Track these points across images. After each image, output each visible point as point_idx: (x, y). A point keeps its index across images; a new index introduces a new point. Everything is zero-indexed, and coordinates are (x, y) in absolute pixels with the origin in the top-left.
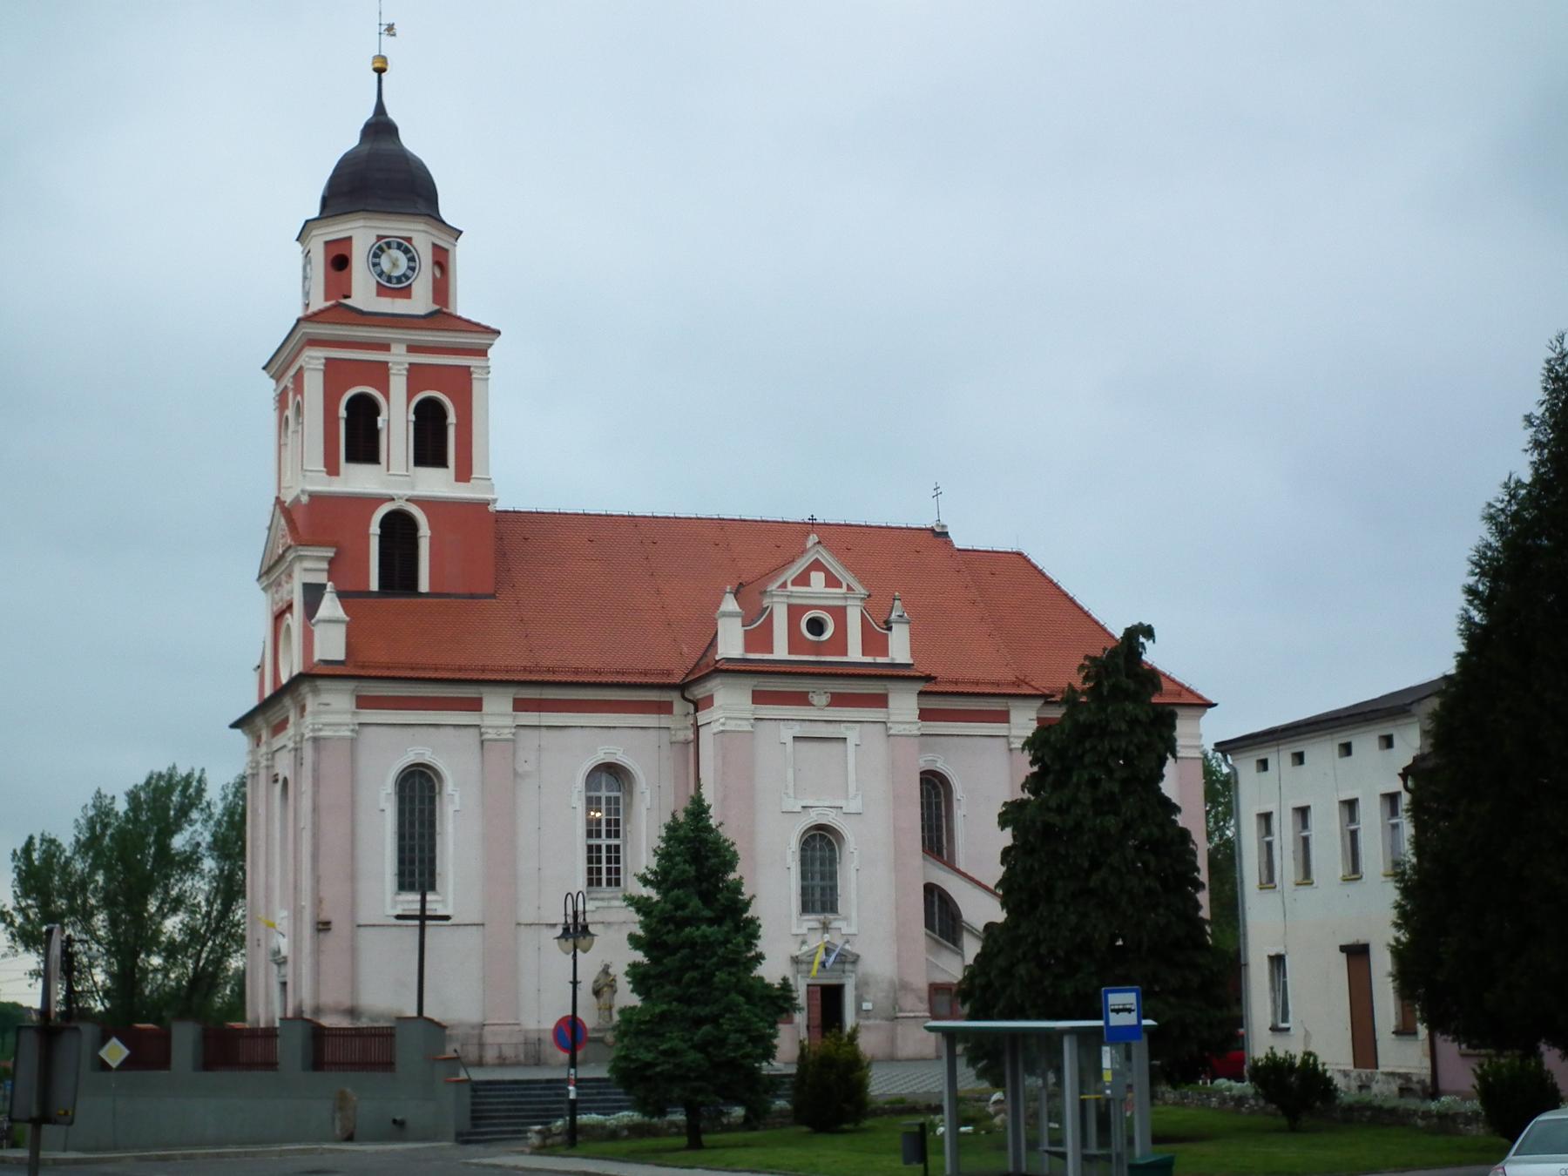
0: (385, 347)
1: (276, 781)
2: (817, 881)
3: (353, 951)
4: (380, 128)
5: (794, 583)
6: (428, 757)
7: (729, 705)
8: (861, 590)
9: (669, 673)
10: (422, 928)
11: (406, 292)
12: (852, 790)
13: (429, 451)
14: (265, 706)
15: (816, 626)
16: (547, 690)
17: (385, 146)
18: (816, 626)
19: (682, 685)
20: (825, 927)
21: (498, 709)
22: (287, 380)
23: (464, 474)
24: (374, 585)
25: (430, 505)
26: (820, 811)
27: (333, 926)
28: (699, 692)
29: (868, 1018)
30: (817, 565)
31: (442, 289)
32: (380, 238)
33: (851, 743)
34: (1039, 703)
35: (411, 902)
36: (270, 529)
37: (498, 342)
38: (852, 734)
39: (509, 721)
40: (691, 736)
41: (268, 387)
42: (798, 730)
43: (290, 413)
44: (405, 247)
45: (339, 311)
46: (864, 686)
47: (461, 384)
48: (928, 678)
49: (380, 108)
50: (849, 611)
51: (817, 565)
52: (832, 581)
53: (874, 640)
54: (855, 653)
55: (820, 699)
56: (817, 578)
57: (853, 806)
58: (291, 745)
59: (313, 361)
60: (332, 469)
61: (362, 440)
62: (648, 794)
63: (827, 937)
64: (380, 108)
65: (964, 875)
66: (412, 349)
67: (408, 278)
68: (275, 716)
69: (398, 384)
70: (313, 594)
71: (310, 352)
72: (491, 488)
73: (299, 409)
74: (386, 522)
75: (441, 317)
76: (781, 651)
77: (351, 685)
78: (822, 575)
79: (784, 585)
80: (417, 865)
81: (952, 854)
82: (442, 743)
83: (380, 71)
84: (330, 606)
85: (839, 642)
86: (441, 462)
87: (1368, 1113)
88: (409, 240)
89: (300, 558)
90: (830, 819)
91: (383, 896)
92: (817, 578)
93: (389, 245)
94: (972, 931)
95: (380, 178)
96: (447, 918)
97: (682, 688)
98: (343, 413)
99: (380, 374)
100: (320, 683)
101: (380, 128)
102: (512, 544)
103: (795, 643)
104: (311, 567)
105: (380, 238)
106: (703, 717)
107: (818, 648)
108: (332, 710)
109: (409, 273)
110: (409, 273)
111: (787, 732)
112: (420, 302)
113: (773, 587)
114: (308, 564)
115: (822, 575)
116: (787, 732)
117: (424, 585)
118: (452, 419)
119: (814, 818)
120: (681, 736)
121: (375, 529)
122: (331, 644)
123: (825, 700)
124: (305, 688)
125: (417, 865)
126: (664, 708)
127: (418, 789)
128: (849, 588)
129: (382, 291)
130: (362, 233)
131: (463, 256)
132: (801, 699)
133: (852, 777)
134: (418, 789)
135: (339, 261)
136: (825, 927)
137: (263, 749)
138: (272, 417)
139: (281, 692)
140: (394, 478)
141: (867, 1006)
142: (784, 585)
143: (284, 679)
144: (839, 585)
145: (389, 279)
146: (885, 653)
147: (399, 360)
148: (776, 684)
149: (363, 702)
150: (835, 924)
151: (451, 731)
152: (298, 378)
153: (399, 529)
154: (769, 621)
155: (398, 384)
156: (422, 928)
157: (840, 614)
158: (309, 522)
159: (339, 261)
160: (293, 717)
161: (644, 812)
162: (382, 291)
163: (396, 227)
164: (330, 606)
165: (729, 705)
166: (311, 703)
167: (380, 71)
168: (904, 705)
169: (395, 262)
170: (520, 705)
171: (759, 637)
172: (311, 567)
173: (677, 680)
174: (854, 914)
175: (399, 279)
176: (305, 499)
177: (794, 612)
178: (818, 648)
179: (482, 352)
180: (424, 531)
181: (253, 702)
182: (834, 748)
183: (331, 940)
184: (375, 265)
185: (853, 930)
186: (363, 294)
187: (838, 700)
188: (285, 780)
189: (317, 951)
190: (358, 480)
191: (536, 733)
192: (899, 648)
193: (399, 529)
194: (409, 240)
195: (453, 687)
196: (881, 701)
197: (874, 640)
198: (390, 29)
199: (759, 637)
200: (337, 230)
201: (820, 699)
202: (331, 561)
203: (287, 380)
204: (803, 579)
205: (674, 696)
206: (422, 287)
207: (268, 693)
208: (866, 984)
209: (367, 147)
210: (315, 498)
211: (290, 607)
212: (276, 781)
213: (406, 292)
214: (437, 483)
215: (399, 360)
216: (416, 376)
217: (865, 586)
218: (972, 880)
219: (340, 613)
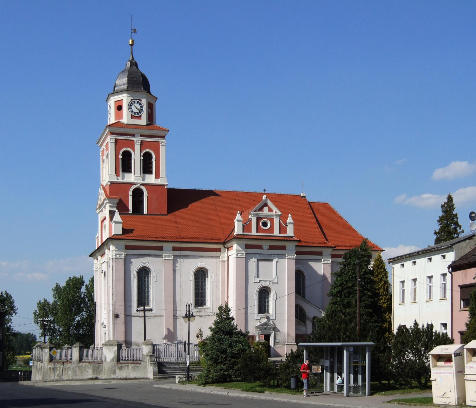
0: (133, 135)
11: (139, 117)
13: (147, 169)
15: (265, 224)
53: (282, 229)
54: (276, 233)
56: (266, 209)
58: (106, 261)
66: (142, 136)
90: (267, 284)
93: (134, 102)
98: (120, 156)
99: (131, 145)
103: (258, 229)
117: (145, 212)
119: (262, 284)
121: (131, 193)
128: (276, 212)
129: (132, 117)
132: (260, 247)
140: (134, 177)
145: (135, 113)
157: (272, 220)
162: (132, 117)
171: (246, 227)
177: (258, 219)
180: (145, 194)
187: (271, 248)
188: (105, 272)
193: (138, 194)
197: (282, 229)
198: (135, 31)
204: (261, 209)
205: (221, 246)
206: (144, 115)
213: (139, 117)
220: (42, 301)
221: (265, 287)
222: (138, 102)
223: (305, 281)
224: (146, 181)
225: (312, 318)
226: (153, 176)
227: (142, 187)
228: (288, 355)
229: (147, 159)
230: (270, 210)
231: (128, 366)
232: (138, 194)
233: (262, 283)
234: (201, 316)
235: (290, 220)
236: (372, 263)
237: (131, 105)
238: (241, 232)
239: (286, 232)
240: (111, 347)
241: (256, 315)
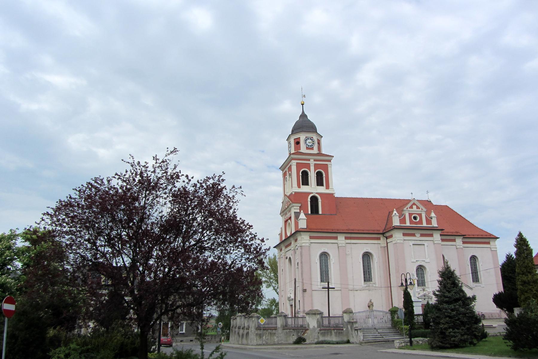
0: (309, 160)
1: (287, 258)
2: (420, 279)
3: (312, 296)
4: (303, 116)
6: (326, 250)
7: (398, 236)
8: (425, 210)
9: (379, 231)
10: (328, 291)
11: (312, 149)
12: (427, 257)
13: (320, 182)
14: (282, 242)
15: (415, 218)
16: (352, 234)
17: (305, 119)
19: (385, 232)
20: (424, 290)
21: (341, 239)
22: (287, 169)
23: (328, 187)
24: (310, 212)
25: (319, 194)
28: (388, 234)
31: (319, 149)
33: (426, 245)
34: (462, 237)
35: (326, 285)
36: (283, 203)
37: (333, 158)
38: (426, 243)
39: (344, 242)
40: (386, 245)
41: (281, 173)
43: (288, 176)
44: (311, 139)
45: (298, 153)
46: (428, 232)
47: (326, 168)
48: (442, 230)
49: (303, 112)
52: (418, 208)
53: (429, 221)
54: (425, 224)
55: (418, 235)
56: (414, 207)
57: (427, 260)
58: (292, 249)
59: (294, 163)
60: (299, 187)
61: (305, 180)
63: (425, 292)
64: (303, 112)
66: (315, 160)
68: (287, 243)
69: (312, 168)
70: (297, 215)
71: (293, 161)
72: (334, 191)
73: (290, 175)
75: (320, 154)
76: (408, 224)
77: (308, 233)
80: (325, 276)
82: (328, 246)
83: (303, 104)
84: (302, 216)
85: (421, 222)
86: (322, 185)
89: (293, 206)
91: (317, 283)
92: (414, 207)
95: (304, 125)
96: (334, 288)
97: (383, 234)
98: (301, 174)
99: (308, 166)
100: (302, 233)
101: (303, 116)
102: (338, 204)
103: (411, 222)
104: (295, 208)
106: (389, 240)
107: (416, 223)
108: (304, 239)
112: (315, 151)
113: (405, 209)
114: (295, 208)
116: (411, 243)
117: (320, 212)
118: (324, 175)
120: (383, 245)
121: (309, 200)
122: (303, 224)
123: (419, 235)
124: (298, 234)
125: (325, 276)
126: (379, 239)
127: (324, 256)
129: (307, 148)
130: (302, 137)
131: (323, 141)
132: (414, 235)
133: (427, 254)
134: (324, 256)
135: (298, 143)
136: (424, 290)
137: (283, 251)
138: (282, 178)
139: (287, 238)
140: (313, 188)
143: (289, 235)
147: (312, 163)
148: (409, 231)
149: (311, 238)
150: (426, 289)
152: (290, 169)
153: (314, 200)
154: (405, 217)
155: (312, 168)
156: (328, 291)
157: (420, 215)
158: (294, 198)
159: (298, 143)
160: (293, 242)
162: (307, 148)
163: (310, 135)
164: (302, 216)
165: (398, 236)
166: (299, 238)
167: (303, 104)
168: (437, 236)
170: (346, 238)
171: (403, 221)
172: (295, 208)
173: (381, 232)
176: (293, 193)
177: (410, 215)
178: (416, 223)
179: (330, 161)
180: (320, 200)
181: (278, 242)
182: (422, 246)
183: (306, 294)
186: (303, 149)
187: (422, 235)
188: (290, 258)
189: (303, 297)
190: (304, 189)
191: (350, 245)
192: (434, 224)
193: (314, 200)
195: (331, 233)
196: (431, 235)
197: (429, 221)
198: (304, 96)
199: (403, 221)
200: (296, 136)
201: (418, 235)
202: (300, 207)
203: (287, 169)
204: (411, 207)
205: (381, 236)
206: (316, 147)
207: (284, 238)
209: (301, 120)
210: (295, 193)
211: (290, 218)
212: (287, 258)
213: (312, 149)
214: (322, 190)
215: (312, 163)
216: (316, 166)
217: (426, 208)
219: (304, 217)
221: (420, 266)
224: (319, 191)
227: (317, 195)
228: (24, 240)
229: (319, 176)
231: (331, 332)
233: (419, 262)
235: (433, 215)
238: (398, 224)
239: (431, 224)
240: (314, 316)
241: (319, 283)
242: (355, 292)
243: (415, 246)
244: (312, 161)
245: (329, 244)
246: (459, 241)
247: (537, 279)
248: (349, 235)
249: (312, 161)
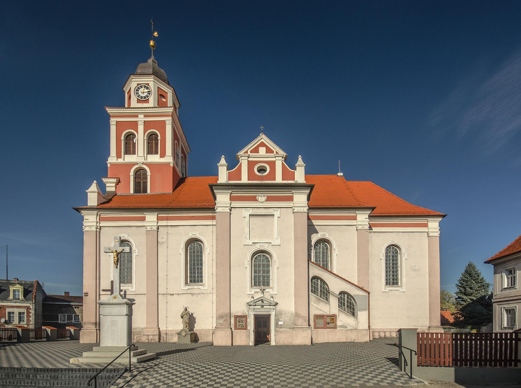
5: (251, 152)
11: (147, 101)
13: (152, 149)
18: (262, 170)
20: (263, 291)
21: (151, 218)
25: (149, 165)
26: (261, 244)
27: (89, 294)
29: (281, 328)
30: (262, 145)
32: (138, 84)
38: (277, 213)
42: (251, 211)
44: (147, 86)
50: (277, 162)
51: (262, 145)
52: (269, 150)
54: (279, 179)
56: (262, 151)
62: (208, 248)
65: (334, 274)
67: (148, 97)
69: (141, 128)
74: (137, 172)
76: (245, 179)
78: (265, 148)
79: (247, 152)
81: (331, 268)
86: (156, 153)
87: (265, 263)
88: (148, 84)
90: (266, 247)
92: (262, 151)
93: (141, 87)
94: (334, 295)
99: (135, 125)
105: (138, 84)
107: (262, 178)
109: (148, 95)
110: (148, 95)
111: (246, 213)
115: (265, 148)
116: (246, 213)
119: (258, 247)
121: (132, 173)
128: (277, 153)
129: (139, 101)
141: (280, 323)
142: (247, 152)
144: (273, 152)
145: (142, 97)
146: (294, 180)
151: (135, 228)
155: (141, 128)
157: (272, 164)
161: (207, 254)
162: (139, 101)
169: (143, 92)
174: (275, 286)
175: (145, 97)
177: (251, 165)
178: (262, 178)
180: (149, 173)
184: (137, 93)
185: (275, 292)
190: (129, 159)
193: (140, 174)
194: (148, 84)
204: (256, 150)
208: (281, 314)
213: (147, 101)
215: (141, 119)
218: (347, 281)
220: (135, 302)
222: (145, 87)
223: (333, 251)
225: (338, 294)
226: (158, 156)
230: (269, 150)
232: (140, 174)
234: (193, 294)
236: (467, 330)
237: (137, 90)
242: (169, 296)
243: (253, 219)
244: (141, 116)
245: (132, 228)
246: (363, 218)
247: (520, 336)
248: (500, 303)
249: (141, 116)
